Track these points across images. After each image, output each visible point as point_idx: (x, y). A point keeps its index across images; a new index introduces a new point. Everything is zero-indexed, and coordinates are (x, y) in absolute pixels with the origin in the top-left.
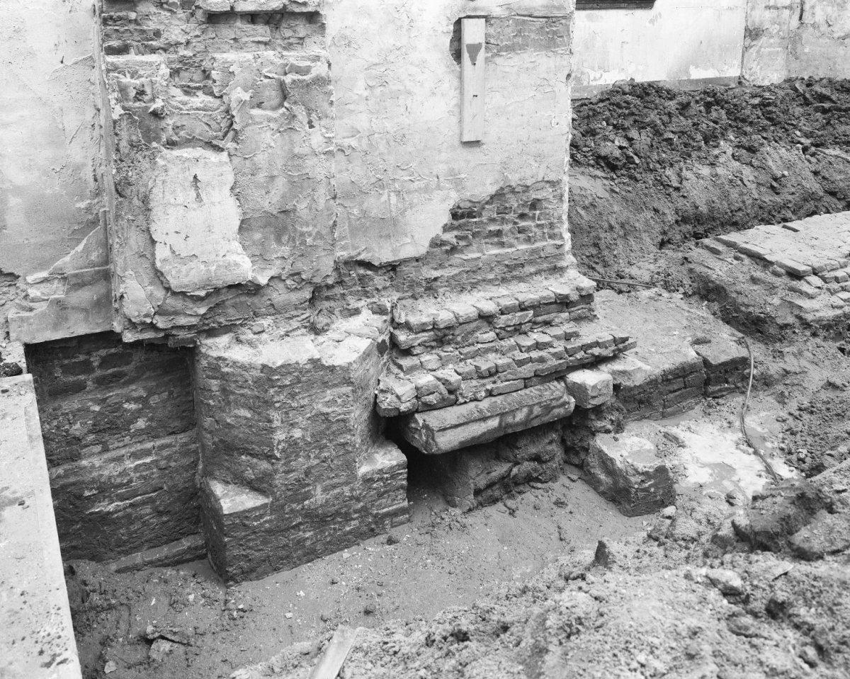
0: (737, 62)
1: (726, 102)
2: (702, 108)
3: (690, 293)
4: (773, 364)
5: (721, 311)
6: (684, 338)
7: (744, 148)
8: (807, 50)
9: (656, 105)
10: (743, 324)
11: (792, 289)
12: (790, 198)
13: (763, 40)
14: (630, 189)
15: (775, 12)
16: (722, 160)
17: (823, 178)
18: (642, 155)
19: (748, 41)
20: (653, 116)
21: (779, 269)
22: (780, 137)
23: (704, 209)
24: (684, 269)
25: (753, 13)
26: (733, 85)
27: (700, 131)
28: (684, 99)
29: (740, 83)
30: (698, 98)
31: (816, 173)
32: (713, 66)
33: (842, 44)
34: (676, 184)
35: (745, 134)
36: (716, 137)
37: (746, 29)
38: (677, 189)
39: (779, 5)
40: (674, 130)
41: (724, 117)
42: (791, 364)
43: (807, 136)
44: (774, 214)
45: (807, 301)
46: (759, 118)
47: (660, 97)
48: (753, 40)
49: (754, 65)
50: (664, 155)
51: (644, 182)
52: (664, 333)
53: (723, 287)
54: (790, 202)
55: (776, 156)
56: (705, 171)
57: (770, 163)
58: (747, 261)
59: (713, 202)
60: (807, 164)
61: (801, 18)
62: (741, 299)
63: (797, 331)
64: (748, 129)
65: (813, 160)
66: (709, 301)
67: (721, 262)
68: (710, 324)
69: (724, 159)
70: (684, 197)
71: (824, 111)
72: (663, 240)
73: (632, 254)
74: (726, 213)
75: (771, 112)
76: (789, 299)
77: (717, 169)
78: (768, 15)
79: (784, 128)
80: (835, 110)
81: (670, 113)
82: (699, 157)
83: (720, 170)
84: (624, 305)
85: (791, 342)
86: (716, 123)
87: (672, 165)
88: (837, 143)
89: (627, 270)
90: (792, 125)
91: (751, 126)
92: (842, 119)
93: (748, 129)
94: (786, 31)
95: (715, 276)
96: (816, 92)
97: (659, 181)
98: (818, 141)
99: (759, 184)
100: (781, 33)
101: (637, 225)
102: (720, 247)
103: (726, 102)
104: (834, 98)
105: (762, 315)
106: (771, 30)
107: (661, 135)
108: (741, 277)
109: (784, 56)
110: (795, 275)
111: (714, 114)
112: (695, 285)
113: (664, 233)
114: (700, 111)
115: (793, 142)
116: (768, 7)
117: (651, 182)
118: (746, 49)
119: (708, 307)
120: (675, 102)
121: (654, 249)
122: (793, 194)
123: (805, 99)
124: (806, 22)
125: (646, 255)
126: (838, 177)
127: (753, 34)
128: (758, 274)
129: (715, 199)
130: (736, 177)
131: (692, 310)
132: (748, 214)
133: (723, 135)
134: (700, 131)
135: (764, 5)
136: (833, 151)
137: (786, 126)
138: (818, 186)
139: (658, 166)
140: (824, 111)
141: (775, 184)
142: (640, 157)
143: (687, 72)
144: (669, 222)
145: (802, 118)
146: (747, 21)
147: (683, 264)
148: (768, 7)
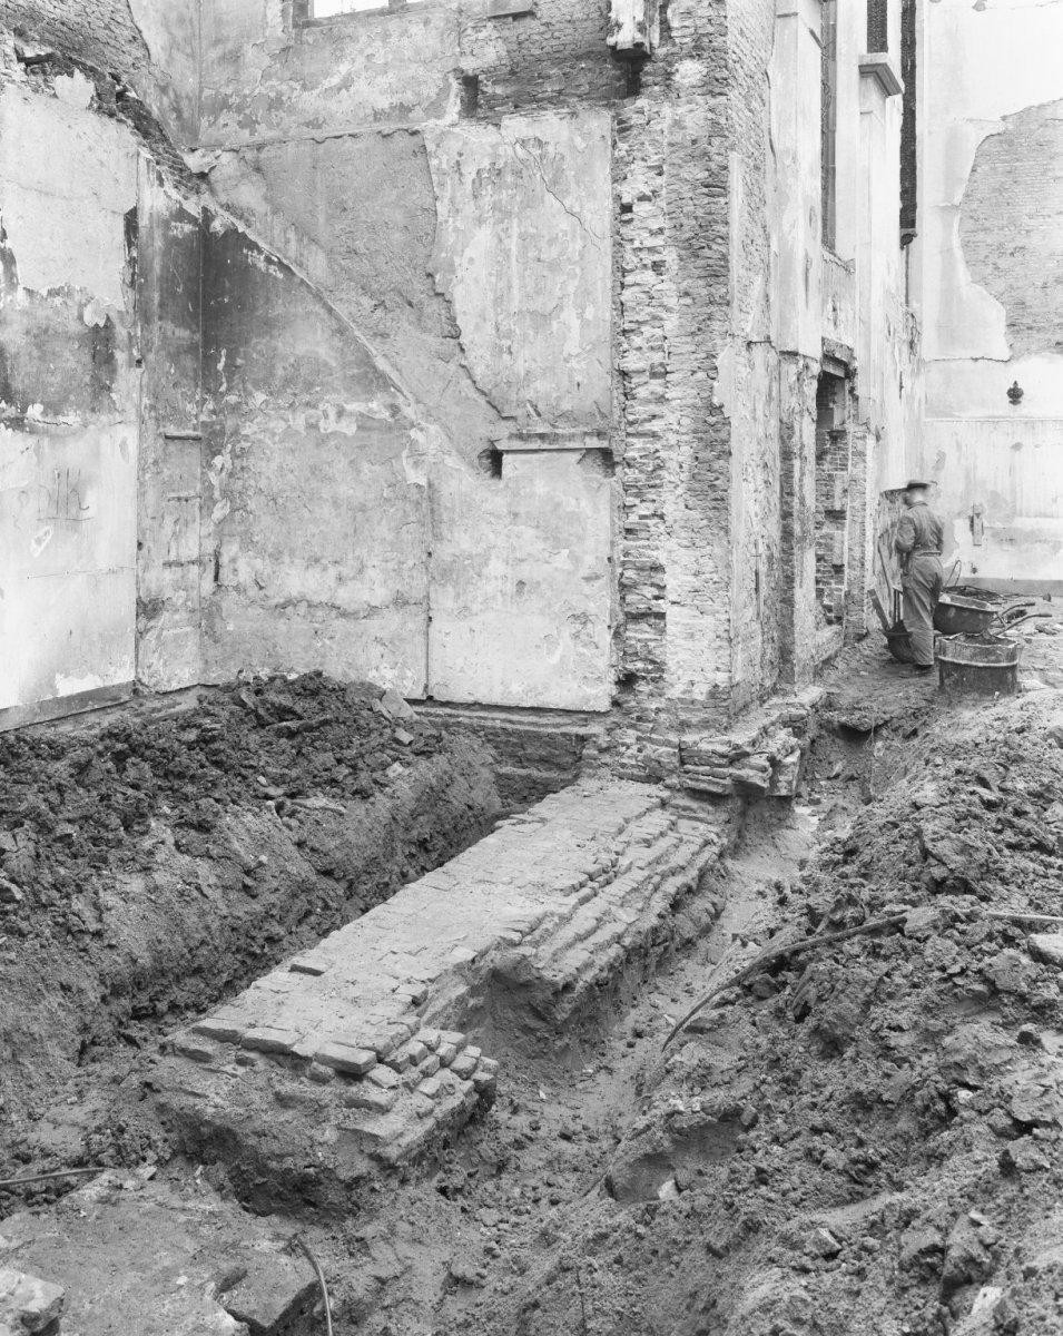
0: (129, 658)
1: (148, 747)
2: (110, 765)
3: (167, 1157)
4: (356, 1273)
5: (231, 1179)
6: (201, 1287)
7: (191, 825)
8: (230, 628)
9: (35, 774)
10: (279, 1195)
11: (353, 1104)
12: (273, 898)
13: (165, 617)
14: (12, 955)
15: (179, 569)
16: (160, 857)
17: (313, 850)
18: (25, 879)
19: (143, 620)
20: (32, 799)
21: (322, 1069)
22: (239, 793)
23: (145, 960)
24: (147, 1108)
25: (147, 575)
26: (126, 698)
27: (115, 810)
28: (80, 755)
29: (135, 691)
30: (100, 747)
31: (300, 845)
32: (91, 670)
33: (282, 615)
34: (93, 926)
35: (186, 798)
36: (143, 816)
37: (139, 602)
38: (98, 934)
39: (183, 560)
40: (70, 816)
41: (149, 775)
42: (384, 1260)
43: (276, 782)
44: (254, 934)
45: (382, 1119)
46: (202, 766)
47: (38, 756)
48: (150, 618)
49: (154, 659)
50: (62, 871)
51: (37, 936)
52: (157, 1288)
53: (229, 1130)
54: (274, 905)
55: (240, 830)
56: (136, 884)
57: (236, 845)
58: (261, 1063)
59: (160, 941)
60: (287, 831)
61: (216, 578)
62: (267, 1146)
63: (377, 1186)
64: (190, 789)
65: (294, 823)
66: (204, 1163)
67: (214, 1076)
68: (229, 1226)
69: (163, 856)
70: (111, 947)
71: (291, 734)
72: (83, 1043)
73: (33, 1094)
74: (183, 956)
75: (217, 752)
76: (353, 1126)
77: (156, 875)
78: (169, 576)
79: (240, 774)
80: (306, 730)
81: (60, 785)
82: (121, 860)
83: (160, 878)
84: (60, 1244)
85: (373, 1213)
86: (135, 787)
87: (80, 889)
88: (317, 785)
89: (32, 1137)
90: (252, 767)
91: (193, 783)
92: (317, 744)
93: (190, 789)
94: (196, 598)
95: (210, 1110)
96: (273, 704)
97: (62, 925)
98: (293, 787)
99: (225, 888)
100: (189, 603)
101: (35, 1028)
102: (209, 1047)
103: (148, 747)
104: (298, 709)
105: (311, 1170)
106: (174, 599)
107: (50, 831)
108: (258, 1100)
109: (197, 640)
110: (351, 1074)
111: (132, 773)
112: (173, 1136)
113: (85, 1029)
114: (108, 771)
115: (257, 797)
116: (168, 564)
117: (47, 932)
118: (140, 634)
119: (206, 1177)
120: (65, 762)
121: (70, 1068)
122: (277, 890)
123: (258, 717)
124: (226, 583)
125: (59, 1088)
126: (332, 844)
127: (148, 608)
128: (289, 1087)
129: (161, 935)
130: (189, 884)
131: (189, 1205)
132: (216, 948)
133: (151, 807)
134: (115, 810)
135: (161, 561)
136: (318, 801)
137: (243, 771)
138: (306, 866)
139: (55, 894)
140: (291, 734)
141: (249, 881)
142: (20, 885)
143: (52, 686)
144: (92, 1004)
145: (261, 752)
146: (138, 589)
147: (143, 1098)
148: (168, 564)
